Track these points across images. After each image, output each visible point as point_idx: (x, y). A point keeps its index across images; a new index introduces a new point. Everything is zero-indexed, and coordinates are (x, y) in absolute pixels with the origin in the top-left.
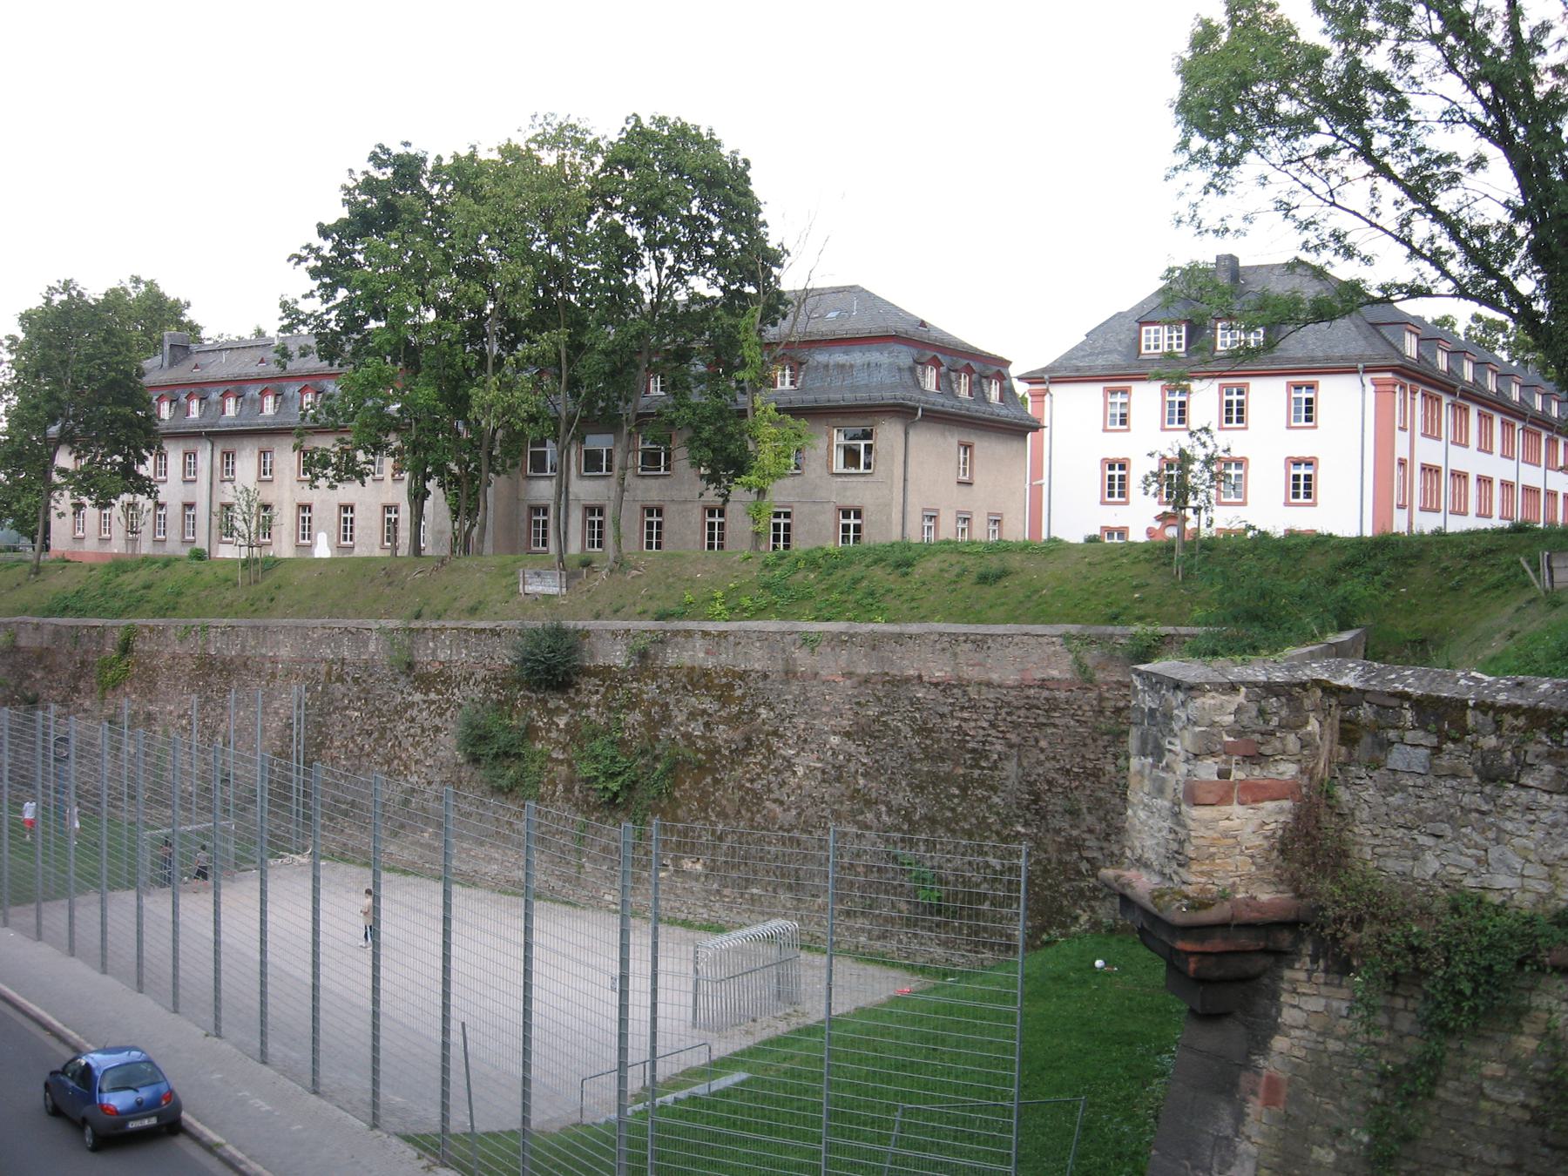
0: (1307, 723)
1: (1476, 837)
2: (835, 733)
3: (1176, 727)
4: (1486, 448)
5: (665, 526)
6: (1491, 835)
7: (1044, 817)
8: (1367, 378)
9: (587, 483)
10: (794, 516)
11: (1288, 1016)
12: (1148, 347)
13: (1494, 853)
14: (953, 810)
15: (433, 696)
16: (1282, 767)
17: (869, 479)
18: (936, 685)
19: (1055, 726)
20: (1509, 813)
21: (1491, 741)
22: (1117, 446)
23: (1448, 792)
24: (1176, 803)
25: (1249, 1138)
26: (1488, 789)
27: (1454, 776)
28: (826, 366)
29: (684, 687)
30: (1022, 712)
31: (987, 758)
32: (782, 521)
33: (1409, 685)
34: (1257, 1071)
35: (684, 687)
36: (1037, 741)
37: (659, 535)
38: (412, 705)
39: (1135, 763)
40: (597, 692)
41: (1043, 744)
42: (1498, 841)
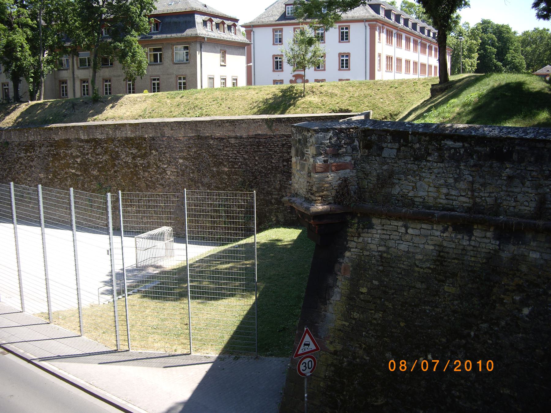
0: (354, 142)
1: (413, 179)
2: (181, 158)
3: (308, 145)
4: (408, 47)
5: (112, 86)
6: (418, 178)
7: (258, 184)
8: (367, 24)
9: (81, 71)
10: (160, 80)
11: (352, 244)
12: (288, 14)
13: (418, 184)
14: (226, 184)
15: (28, 154)
16: (346, 158)
17: (188, 65)
18: (218, 138)
19: (260, 151)
20: (423, 170)
21: (418, 145)
22: (278, 50)
23: (403, 164)
24: (309, 173)
25: (338, 286)
26: (416, 163)
27: (405, 158)
28: (170, 23)
29: (124, 145)
30: (249, 147)
31: (237, 164)
32: (156, 82)
33: (389, 127)
34: (341, 263)
35: (124, 145)
36: (255, 157)
37: (110, 89)
38: (21, 158)
39: (294, 160)
40: (91, 149)
41: (257, 158)
42: (420, 180)
